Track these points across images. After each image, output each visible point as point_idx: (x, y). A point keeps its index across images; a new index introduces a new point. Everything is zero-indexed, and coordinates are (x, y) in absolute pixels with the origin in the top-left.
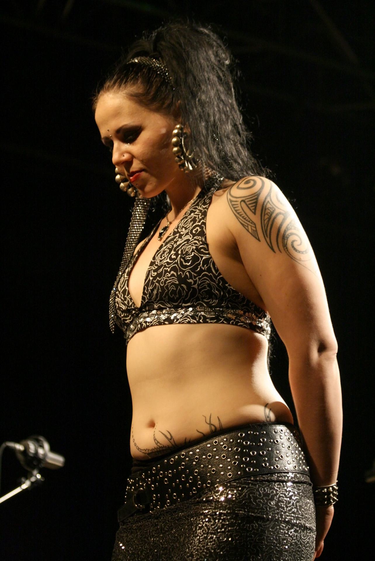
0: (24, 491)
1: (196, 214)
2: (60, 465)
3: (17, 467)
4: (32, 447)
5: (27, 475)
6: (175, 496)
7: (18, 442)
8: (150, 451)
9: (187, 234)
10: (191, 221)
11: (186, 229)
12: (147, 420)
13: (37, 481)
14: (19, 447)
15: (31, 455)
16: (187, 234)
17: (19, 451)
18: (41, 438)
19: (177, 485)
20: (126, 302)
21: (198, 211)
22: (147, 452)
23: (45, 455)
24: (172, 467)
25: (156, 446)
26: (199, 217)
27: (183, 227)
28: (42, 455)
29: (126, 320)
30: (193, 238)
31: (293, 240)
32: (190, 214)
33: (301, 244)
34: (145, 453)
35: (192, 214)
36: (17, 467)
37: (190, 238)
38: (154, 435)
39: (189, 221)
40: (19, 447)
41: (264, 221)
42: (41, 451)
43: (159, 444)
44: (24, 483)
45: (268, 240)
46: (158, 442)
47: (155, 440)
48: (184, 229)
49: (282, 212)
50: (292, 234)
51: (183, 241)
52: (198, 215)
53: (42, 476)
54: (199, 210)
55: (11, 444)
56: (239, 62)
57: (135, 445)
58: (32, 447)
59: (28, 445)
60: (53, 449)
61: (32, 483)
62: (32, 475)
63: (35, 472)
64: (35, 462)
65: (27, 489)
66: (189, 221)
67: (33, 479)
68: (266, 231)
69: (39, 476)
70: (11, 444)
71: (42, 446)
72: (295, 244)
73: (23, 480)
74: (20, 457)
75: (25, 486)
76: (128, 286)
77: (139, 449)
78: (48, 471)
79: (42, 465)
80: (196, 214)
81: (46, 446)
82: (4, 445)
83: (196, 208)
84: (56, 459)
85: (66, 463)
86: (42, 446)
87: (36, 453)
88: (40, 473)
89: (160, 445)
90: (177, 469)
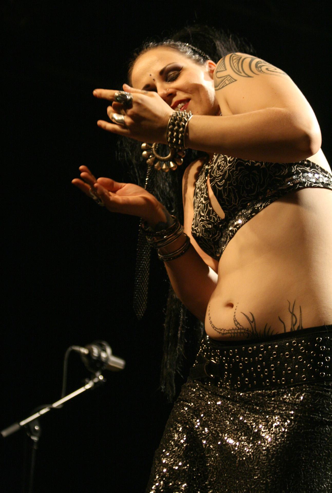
0: (87, 391)
2: (121, 367)
3: (84, 368)
4: (96, 351)
5: (91, 377)
6: (247, 381)
7: (83, 346)
8: (225, 332)
12: (229, 309)
13: (100, 381)
14: (84, 351)
15: (95, 358)
17: (84, 354)
18: (104, 344)
19: (251, 373)
20: (212, 221)
22: (222, 332)
23: (107, 358)
24: (249, 356)
25: (234, 327)
28: (105, 358)
29: (215, 238)
34: (220, 333)
36: (84, 368)
38: (235, 316)
40: (84, 351)
41: (234, 67)
42: (104, 355)
43: (238, 326)
44: (87, 383)
45: (243, 74)
46: (238, 323)
47: (235, 320)
53: (104, 377)
55: (77, 348)
57: (211, 322)
58: (96, 351)
59: (92, 349)
60: (114, 353)
61: (95, 384)
62: (95, 377)
63: (98, 374)
64: (99, 364)
65: (90, 389)
67: (96, 380)
69: (101, 378)
70: (77, 348)
71: (105, 351)
73: (87, 381)
74: (85, 359)
75: (88, 386)
76: (211, 206)
77: (214, 327)
78: (109, 372)
79: (105, 368)
81: (109, 350)
82: (70, 349)
84: (118, 362)
85: (126, 366)
86: (105, 351)
87: (100, 356)
88: (102, 374)
89: (240, 327)
90: (254, 359)
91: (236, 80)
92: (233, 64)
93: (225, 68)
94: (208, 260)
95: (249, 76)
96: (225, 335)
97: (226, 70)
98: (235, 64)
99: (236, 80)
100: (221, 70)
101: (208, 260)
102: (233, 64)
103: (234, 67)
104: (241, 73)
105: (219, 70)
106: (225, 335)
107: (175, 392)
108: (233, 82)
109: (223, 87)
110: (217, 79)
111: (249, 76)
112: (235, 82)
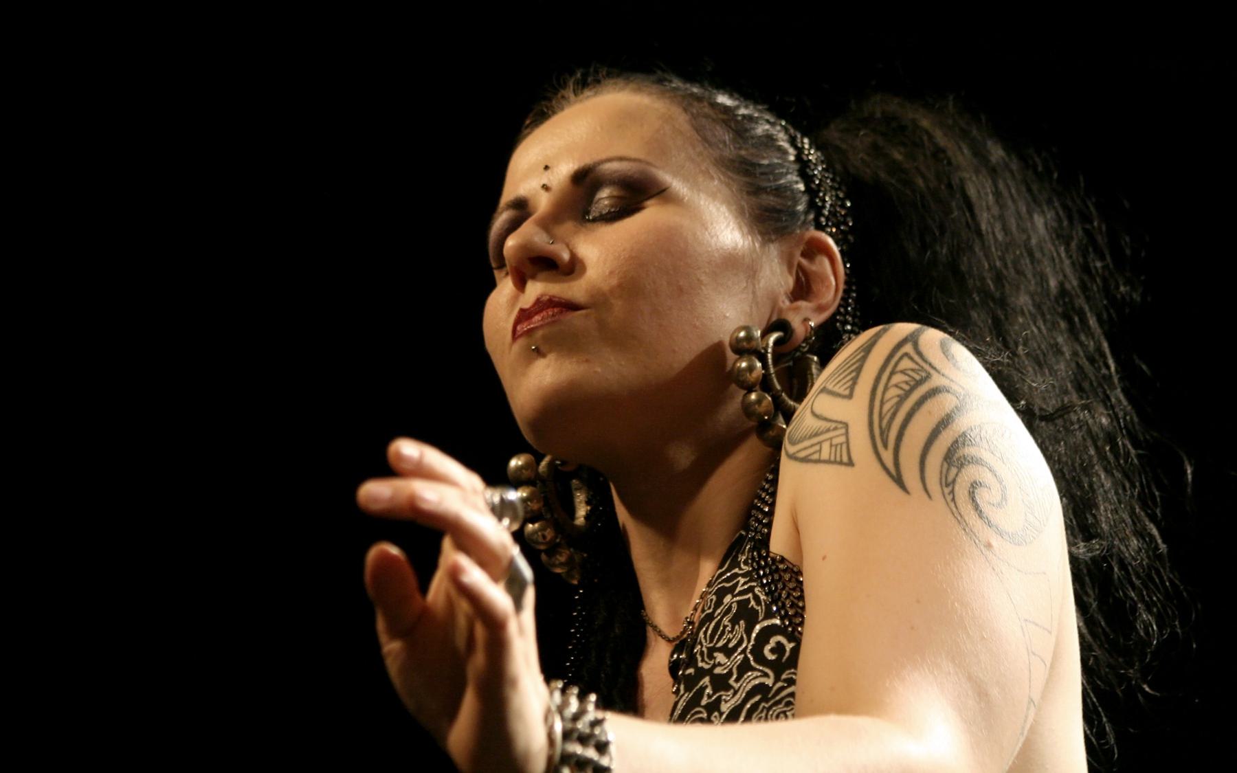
1: (741, 593)
9: (744, 667)
10: (734, 621)
11: (729, 652)
16: (744, 667)
21: (742, 580)
26: (757, 598)
27: (711, 651)
30: (777, 679)
31: (978, 479)
32: (719, 603)
33: (999, 505)
35: (728, 599)
37: (769, 682)
39: (726, 621)
41: (882, 403)
45: (888, 456)
48: (720, 657)
49: (954, 387)
50: (978, 461)
51: (741, 696)
52: (751, 589)
54: (743, 576)
56: (1139, 299)
66: (726, 621)
68: (884, 433)
72: (983, 496)
80: (741, 593)
83: (736, 576)
91: (850, 463)
92: (886, 389)
93: (852, 388)
94: (742, 719)
95: (899, 480)
96: (772, 120)
97: (850, 396)
98: (893, 392)
99: (850, 463)
100: (836, 389)
101: (742, 719)
102: (886, 389)
103: (882, 403)
104: (885, 446)
105: (830, 387)
106: (772, 120)
107: (752, 642)
108: (841, 463)
109: (805, 460)
110: (808, 412)
111: (899, 480)
112: (843, 468)
